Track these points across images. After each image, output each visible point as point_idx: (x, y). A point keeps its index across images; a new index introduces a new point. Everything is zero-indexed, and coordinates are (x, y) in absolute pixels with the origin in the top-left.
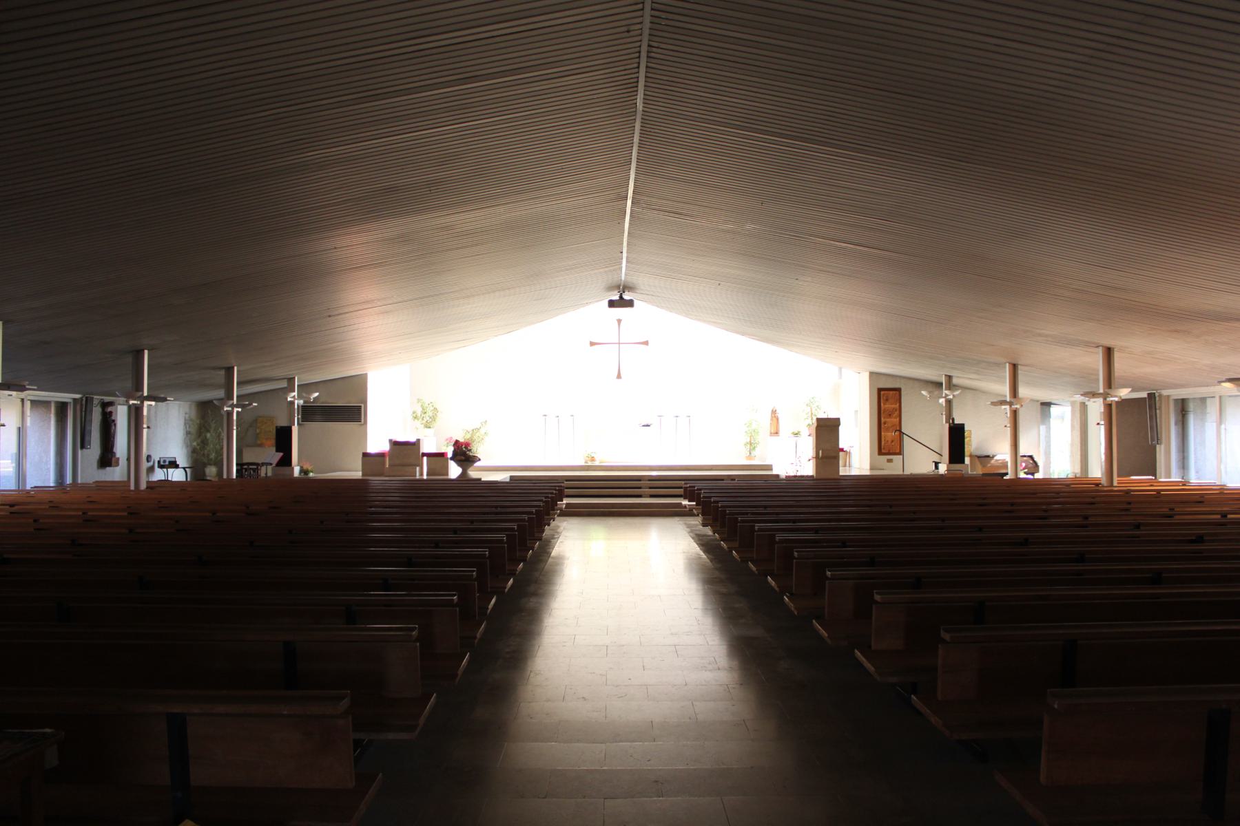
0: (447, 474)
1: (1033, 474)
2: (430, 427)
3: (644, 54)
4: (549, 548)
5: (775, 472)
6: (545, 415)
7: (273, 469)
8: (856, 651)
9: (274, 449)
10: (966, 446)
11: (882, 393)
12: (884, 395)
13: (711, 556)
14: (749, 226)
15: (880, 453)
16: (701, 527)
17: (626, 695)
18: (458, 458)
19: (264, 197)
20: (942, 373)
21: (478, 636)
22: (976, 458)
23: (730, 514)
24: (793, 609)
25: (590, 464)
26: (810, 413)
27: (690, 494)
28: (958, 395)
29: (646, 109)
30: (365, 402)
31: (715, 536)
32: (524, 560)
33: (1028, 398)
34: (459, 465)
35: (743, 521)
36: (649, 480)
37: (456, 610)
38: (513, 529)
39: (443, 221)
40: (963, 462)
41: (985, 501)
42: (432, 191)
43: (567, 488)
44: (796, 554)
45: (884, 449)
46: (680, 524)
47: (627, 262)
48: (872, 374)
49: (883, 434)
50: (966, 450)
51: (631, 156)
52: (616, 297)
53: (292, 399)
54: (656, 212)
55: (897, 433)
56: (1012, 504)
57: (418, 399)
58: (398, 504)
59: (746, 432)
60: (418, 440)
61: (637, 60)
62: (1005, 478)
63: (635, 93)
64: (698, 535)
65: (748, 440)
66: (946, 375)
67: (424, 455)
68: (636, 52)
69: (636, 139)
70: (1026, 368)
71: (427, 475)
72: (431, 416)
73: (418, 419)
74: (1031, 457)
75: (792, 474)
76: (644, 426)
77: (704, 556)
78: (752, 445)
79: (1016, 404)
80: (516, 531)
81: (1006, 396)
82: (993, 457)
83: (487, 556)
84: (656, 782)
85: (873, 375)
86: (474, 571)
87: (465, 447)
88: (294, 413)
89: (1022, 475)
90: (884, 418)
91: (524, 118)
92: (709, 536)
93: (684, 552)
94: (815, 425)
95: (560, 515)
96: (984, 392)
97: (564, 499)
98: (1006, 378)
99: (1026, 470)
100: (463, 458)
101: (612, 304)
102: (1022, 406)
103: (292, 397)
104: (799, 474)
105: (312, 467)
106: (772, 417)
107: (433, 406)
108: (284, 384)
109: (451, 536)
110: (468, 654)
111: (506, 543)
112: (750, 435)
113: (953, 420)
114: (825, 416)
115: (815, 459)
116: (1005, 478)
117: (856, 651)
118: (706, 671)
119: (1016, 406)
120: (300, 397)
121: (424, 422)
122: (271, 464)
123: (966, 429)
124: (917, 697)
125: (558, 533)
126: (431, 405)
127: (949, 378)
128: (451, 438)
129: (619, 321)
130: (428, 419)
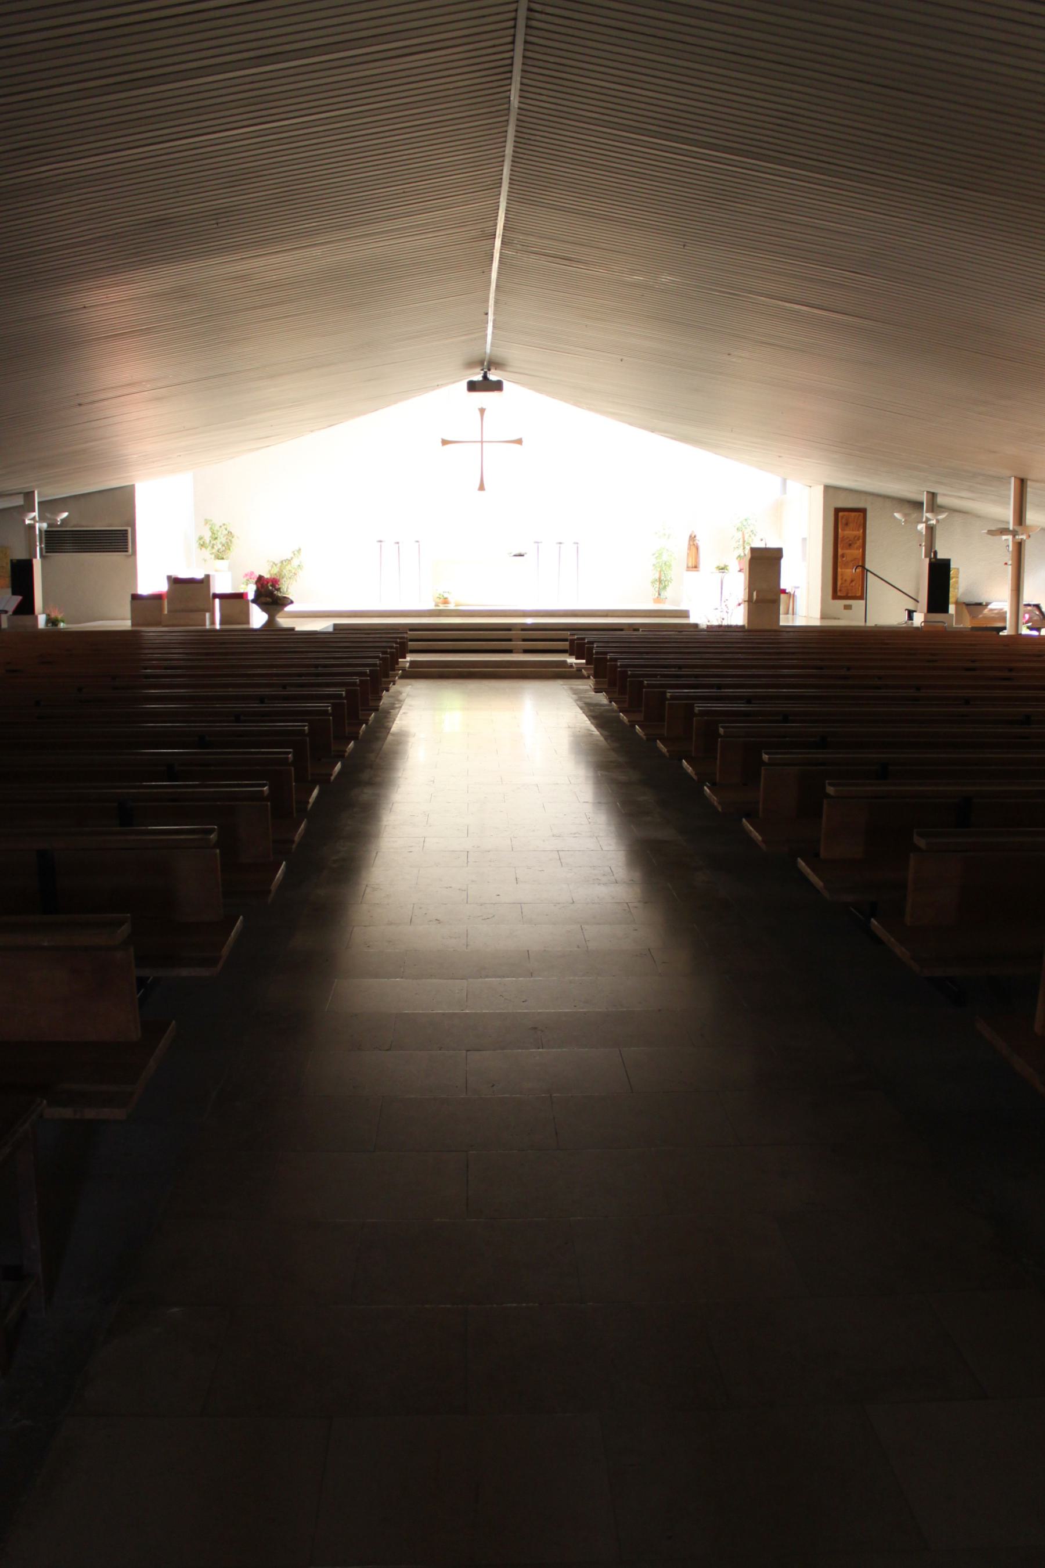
0: (248, 622)
1: (1038, 629)
2: (223, 559)
3: (521, 23)
4: (388, 722)
5: (692, 620)
6: (380, 541)
7: (9, 619)
8: (799, 860)
9: (9, 590)
10: (951, 589)
11: (841, 514)
12: (842, 517)
13: (606, 733)
14: (665, 278)
15: (835, 596)
16: (594, 693)
17: (494, 916)
18: (263, 599)
19: (848, 299)
20: (922, 489)
21: (297, 838)
22: (964, 606)
23: (632, 676)
24: (716, 804)
25: (442, 607)
26: (741, 540)
27: (578, 648)
28: (943, 519)
29: (523, 106)
30: (132, 524)
31: (611, 705)
32: (355, 737)
33: (1039, 527)
34: (264, 610)
35: (649, 686)
36: (523, 630)
37: (267, 805)
38: (340, 697)
39: (232, 269)
40: (945, 610)
41: (977, 664)
42: (220, 225)
43: (411, 640)
44: (721, 731)
45: (840, 590)
46: (572, 698)
47: (494, 327)
48: (827, 488)
49: (839, 570)
50: (951, 595)
51: (502, 174)
52: (478, 378)
53: (32, 522)
54: (533, 256)
55: (859, 570)
56: (1011, 670)
57: (206, 520)
58: (182, 663)
59: (654, 565)
60: (208, 577)
61: (512, 31)
62: (1001, 634)
63: (507, 82)
64: (588, 704)
65: (657, 576)
66: (928, 492)
67: (215, 596)
68: (511, 20)
69: (509, 150)
70: (1038, 485)
71: (221, 624)
72: (224, 542)
73: (206, 548)
74: (1038, 606)
75: (715, 623)
76: (515, 556)
77: (596, 732)
78: (661, 583)
79: (1022, 534)
80: (344, 699)
81: (1008, 523)
82: (987, 604)
83: (307, 732)
84: (535, 1028)
85: (830, 490)
86: (289, 753)
87: (272, 586)
88: (36, 542)
89: (1025, 631)
90: (842, 549)
91: (285, 129)
92: (606, 705)
93: (569, 727)
94: (749, 556)
95: (402, 677)
96: (977, 516)
97: (407, 655)
98: (1010, 498)
99: (1030, 624)
100: (269, 600)
101: (472, 387)
102: (1029, 536)
103: (30, 520)
104: (725, 623)
105: (62, 615)
106: (689, 544)
107: (226, 529)
108: (19, 501)
109: (255, 706)
110: (284, 863)
111: (331, 715)
112: (659, 569)
113: (935, 553)
114: (761, 545)
115: (746, 603)
116: (1001, 634)
117: (799, 860)
118: (599, 884)
119: (1021, 537)
120: (42, 519)
121: (214, 551)
122: (6, 612)
123: (953, 566)
124: (877, 920)
125: (399, 700)
126: (223, 527)
127: (933, 496)
128: (252, 573)
129: (482, 411)
130: (220, 546)
